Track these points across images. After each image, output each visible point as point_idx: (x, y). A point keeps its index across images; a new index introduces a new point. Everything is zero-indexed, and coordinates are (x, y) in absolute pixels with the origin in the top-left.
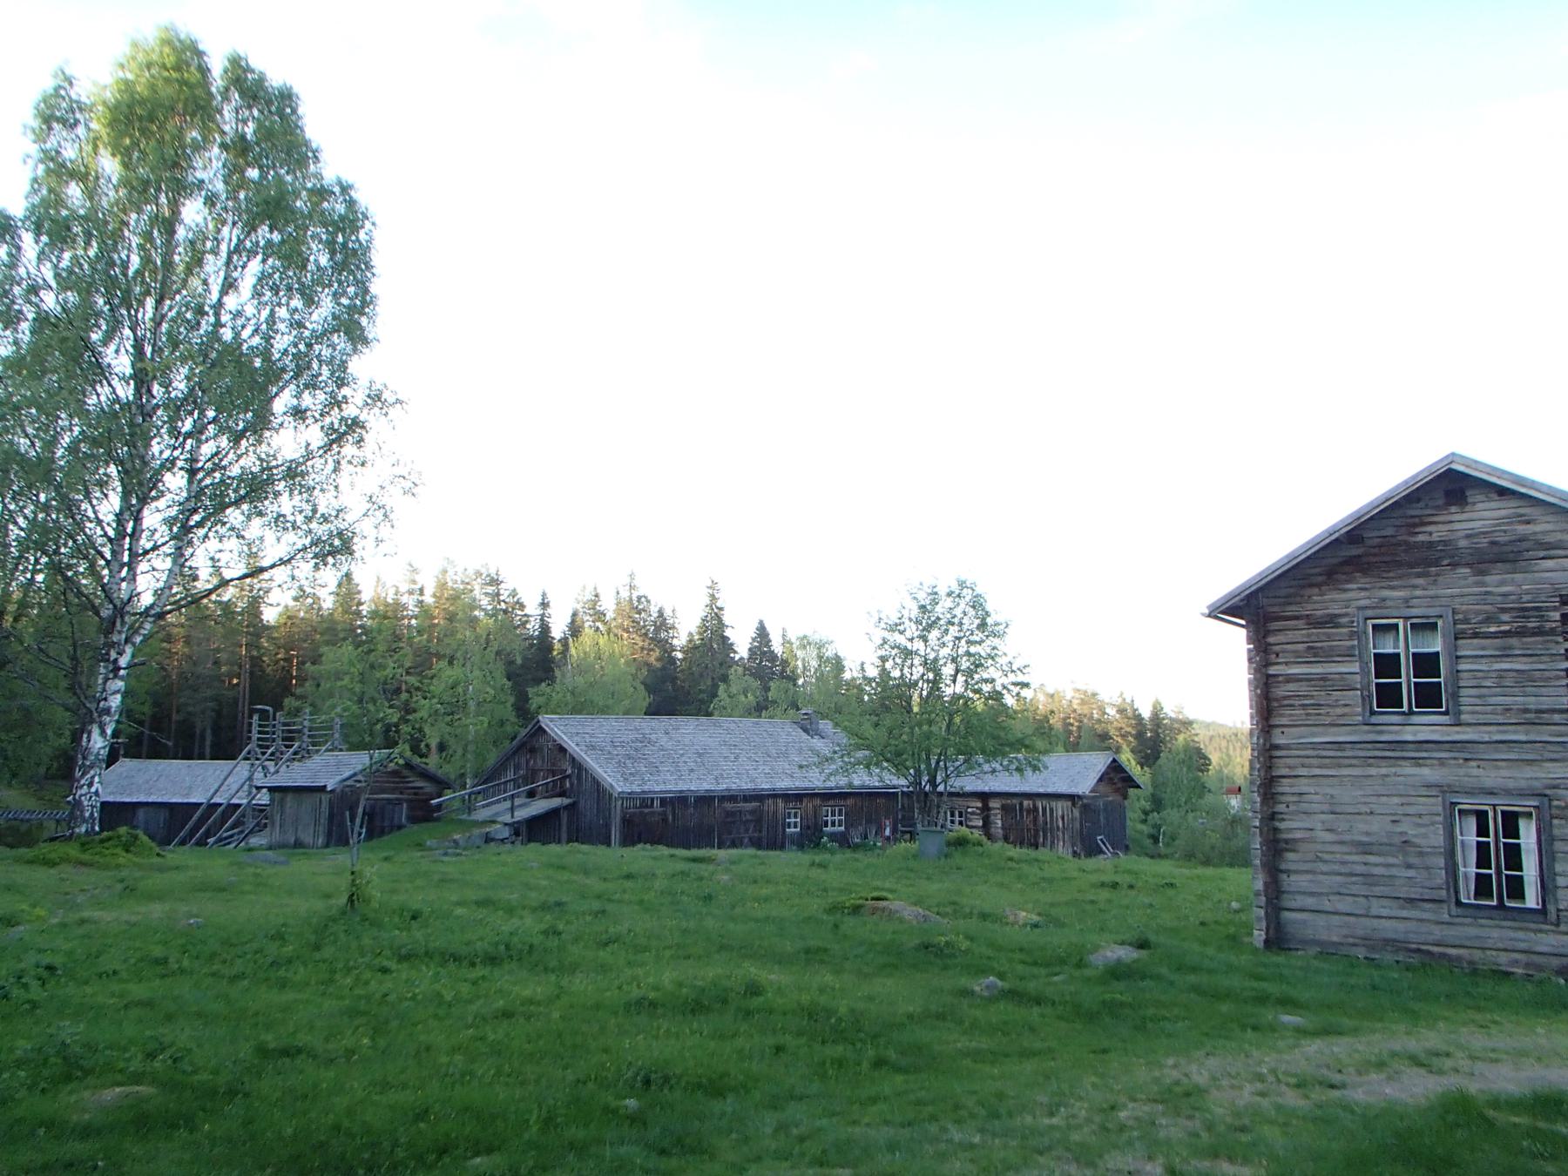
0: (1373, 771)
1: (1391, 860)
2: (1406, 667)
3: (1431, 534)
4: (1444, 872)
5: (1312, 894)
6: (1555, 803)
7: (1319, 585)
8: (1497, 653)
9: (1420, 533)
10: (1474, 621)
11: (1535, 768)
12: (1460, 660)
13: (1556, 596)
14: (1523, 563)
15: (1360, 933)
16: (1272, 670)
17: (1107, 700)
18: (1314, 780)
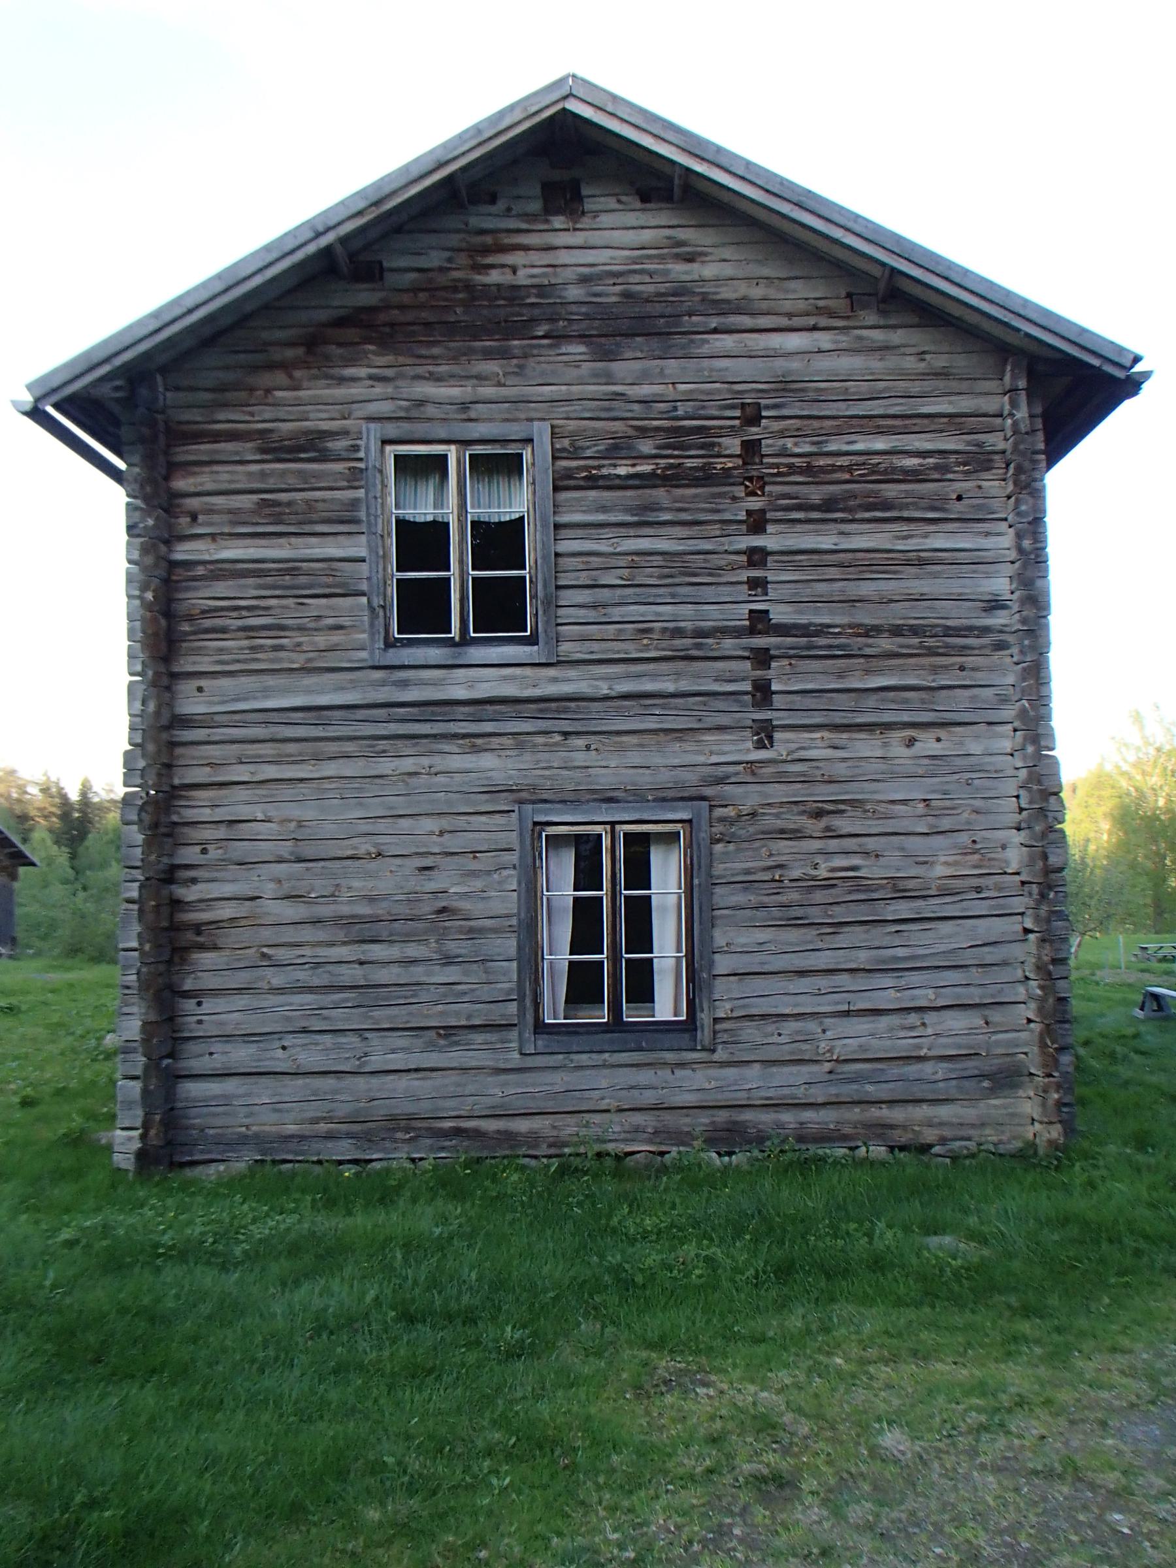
0: (386, 766)
1: (413, 951)
2: (459, 548)
3: (514, 270)
4: (515, 964)
5: (248, 1037)
6: (719, 812)
7: (285, 366)
8: (629, 518)
9: (492, 266)
10: (588, 453)
11: (687, 746)
12: (564, 533)
13: (733, 407)
14: (683, 340)
15: (342, 1110)
16: (183, 552)
17: (29, 778)
18: (261, 791)
